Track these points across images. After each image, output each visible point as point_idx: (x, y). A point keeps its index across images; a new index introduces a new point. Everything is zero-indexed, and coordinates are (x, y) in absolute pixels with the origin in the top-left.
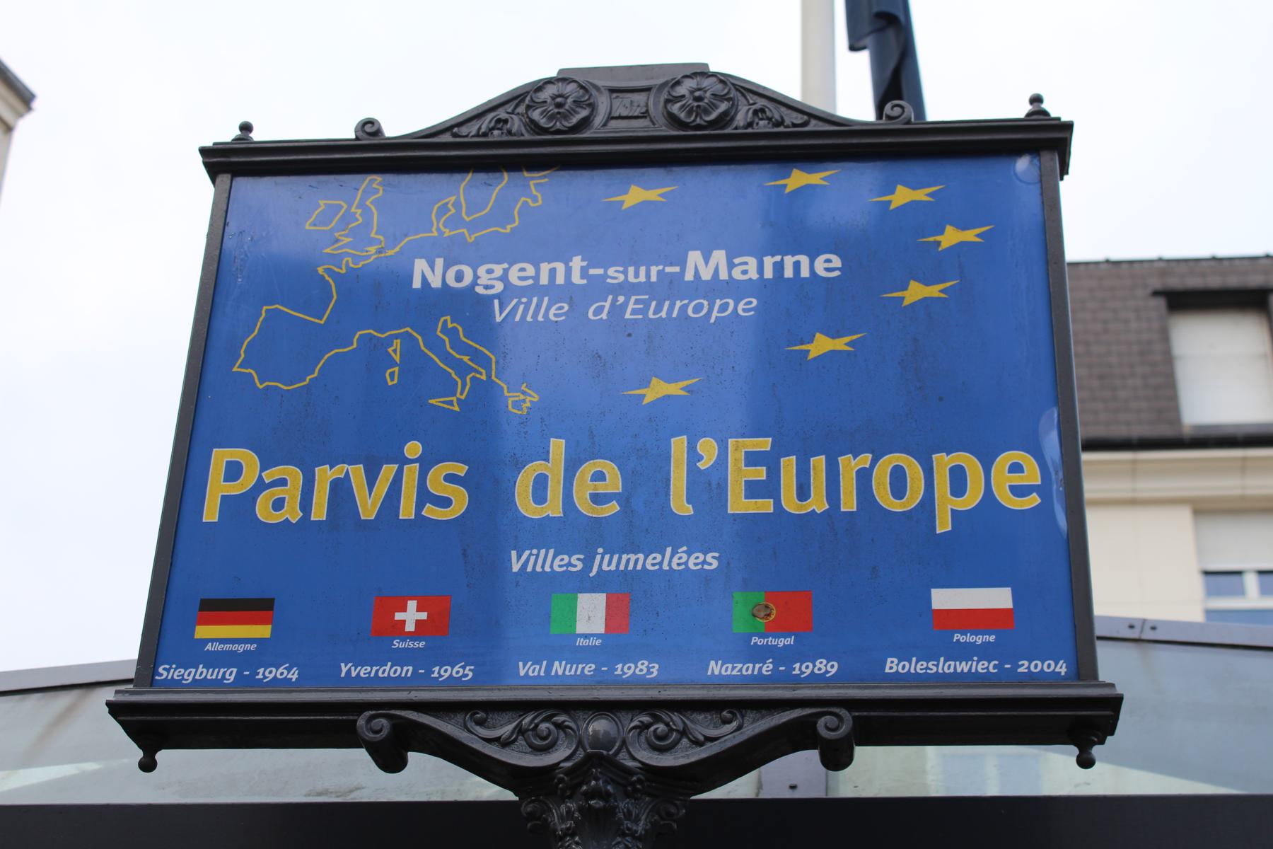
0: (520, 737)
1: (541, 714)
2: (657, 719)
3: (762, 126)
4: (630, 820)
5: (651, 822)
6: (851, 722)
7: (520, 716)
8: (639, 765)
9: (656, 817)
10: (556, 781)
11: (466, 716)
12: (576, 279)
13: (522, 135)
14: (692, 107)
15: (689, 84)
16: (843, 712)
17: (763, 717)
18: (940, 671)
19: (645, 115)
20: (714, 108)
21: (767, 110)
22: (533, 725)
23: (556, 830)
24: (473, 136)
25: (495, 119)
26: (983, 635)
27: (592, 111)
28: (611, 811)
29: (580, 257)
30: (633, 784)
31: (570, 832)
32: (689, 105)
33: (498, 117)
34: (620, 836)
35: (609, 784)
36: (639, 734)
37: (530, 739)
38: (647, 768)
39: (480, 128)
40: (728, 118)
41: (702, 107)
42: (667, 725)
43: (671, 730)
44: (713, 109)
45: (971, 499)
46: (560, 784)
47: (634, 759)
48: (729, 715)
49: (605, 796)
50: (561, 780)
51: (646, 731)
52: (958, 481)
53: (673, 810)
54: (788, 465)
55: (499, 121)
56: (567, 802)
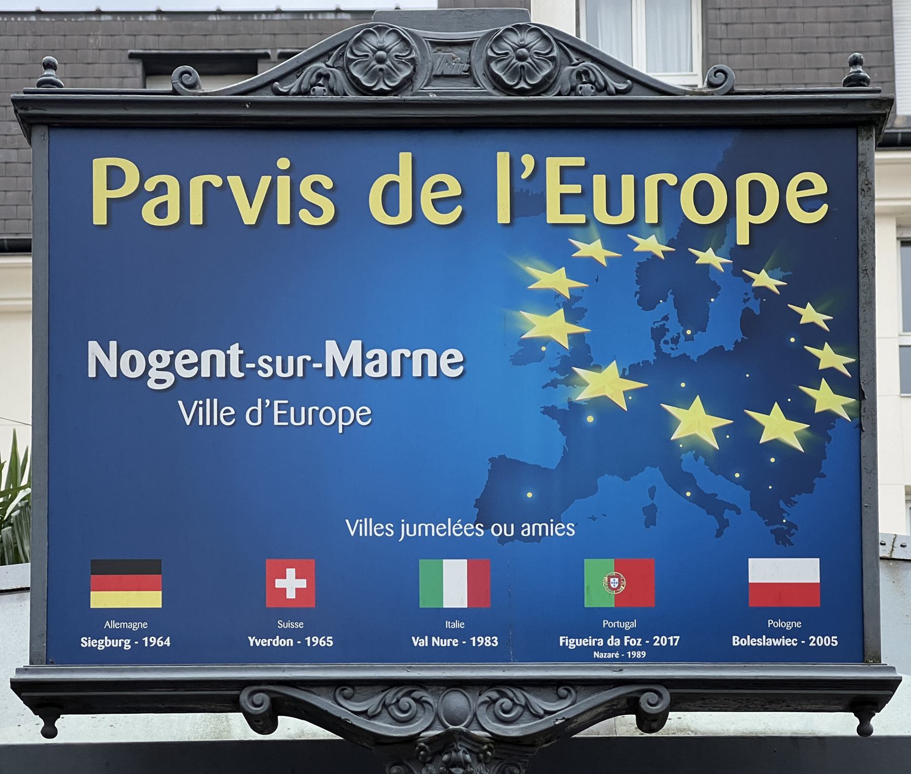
0: (384, 710)
1: (403, 689)
2: (503, 695)
3: (587, 93)
6: (669, 698)
7: (383, 691)
8: (489, 735)
10: (417, 748)
12: (236, 373)
14: (516, 67)
16: (662, 690)
19: (469, 74)
20: (539, 71)
21: (590, 71)
22: (395, 700)
24: (294, 94)
25: (315, 74)
26: (603, 658)
27: (414, 70)
29: (802, 322)
33: (319, 71)
35: (466, 753)
36: (488, 708)
38: (497, 740)
39: (301, 84)
40: (551, 81)
42: (512, 700)
45: (275, 640)
47: (484, 730)
48: (565, 692)
50: (422, 749)
51: (493, 705)
55: (320, 76)
56: (428, 766)
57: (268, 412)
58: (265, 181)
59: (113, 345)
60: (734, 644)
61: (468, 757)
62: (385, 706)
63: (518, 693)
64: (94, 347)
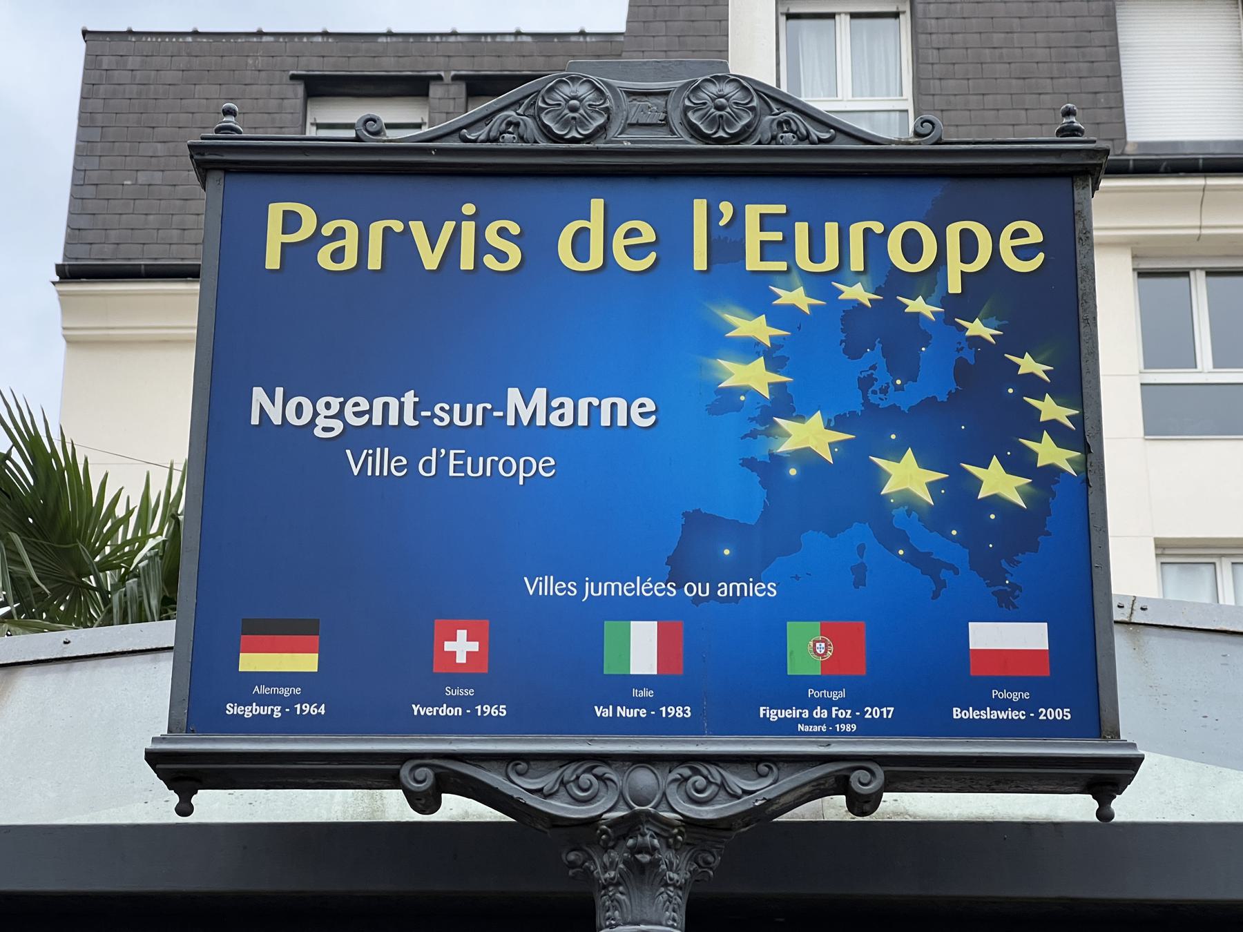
0: (562, 788)
1: (582, 765)
2: (696, 772)
3: (788, 141)
4: (671, 870)
5: (690, 872)
6: (883, 777)
7: (561, 767)
8: (681, 818)
9: (695, 866)
10: (598, 832)
11: (507, 767)
12: (410, 421)
13: (536, 142)
15: (713, 89)
17: (798, 771)
18: (989, 717)
19: (665, 123)
22: (574, 777)
23: (600, 879)
24: (482, 141)
25: (505, 122)
27: (608, 118)
28: (655, 864)
30: (674, 836)
31: (615, 881)
32: (710, 115)
33: (509, 119)
34: (662, 886)
35: (654, 838)
37: (572, 790)
38: (689, 822)
39: (490, 131)
40: (751, 130)
41: (724, 118)
42: (706, 778)
43: (709, 783)
44: (737, 121)
46: (603, 834)
47: (675, 811)
48: (766, 769)
49: (652, 850)
50: (604, 832)
52: (969, 247)
53: (710, 859)
54: (801, 230)
55: (509, 124)
57: (442, 463)
58: (449, 227)
59: (279, 391)
60: (955, 717)
61: (656, 841)
62: (563, 783)
63: (713, 769)
64: (259, 394)
